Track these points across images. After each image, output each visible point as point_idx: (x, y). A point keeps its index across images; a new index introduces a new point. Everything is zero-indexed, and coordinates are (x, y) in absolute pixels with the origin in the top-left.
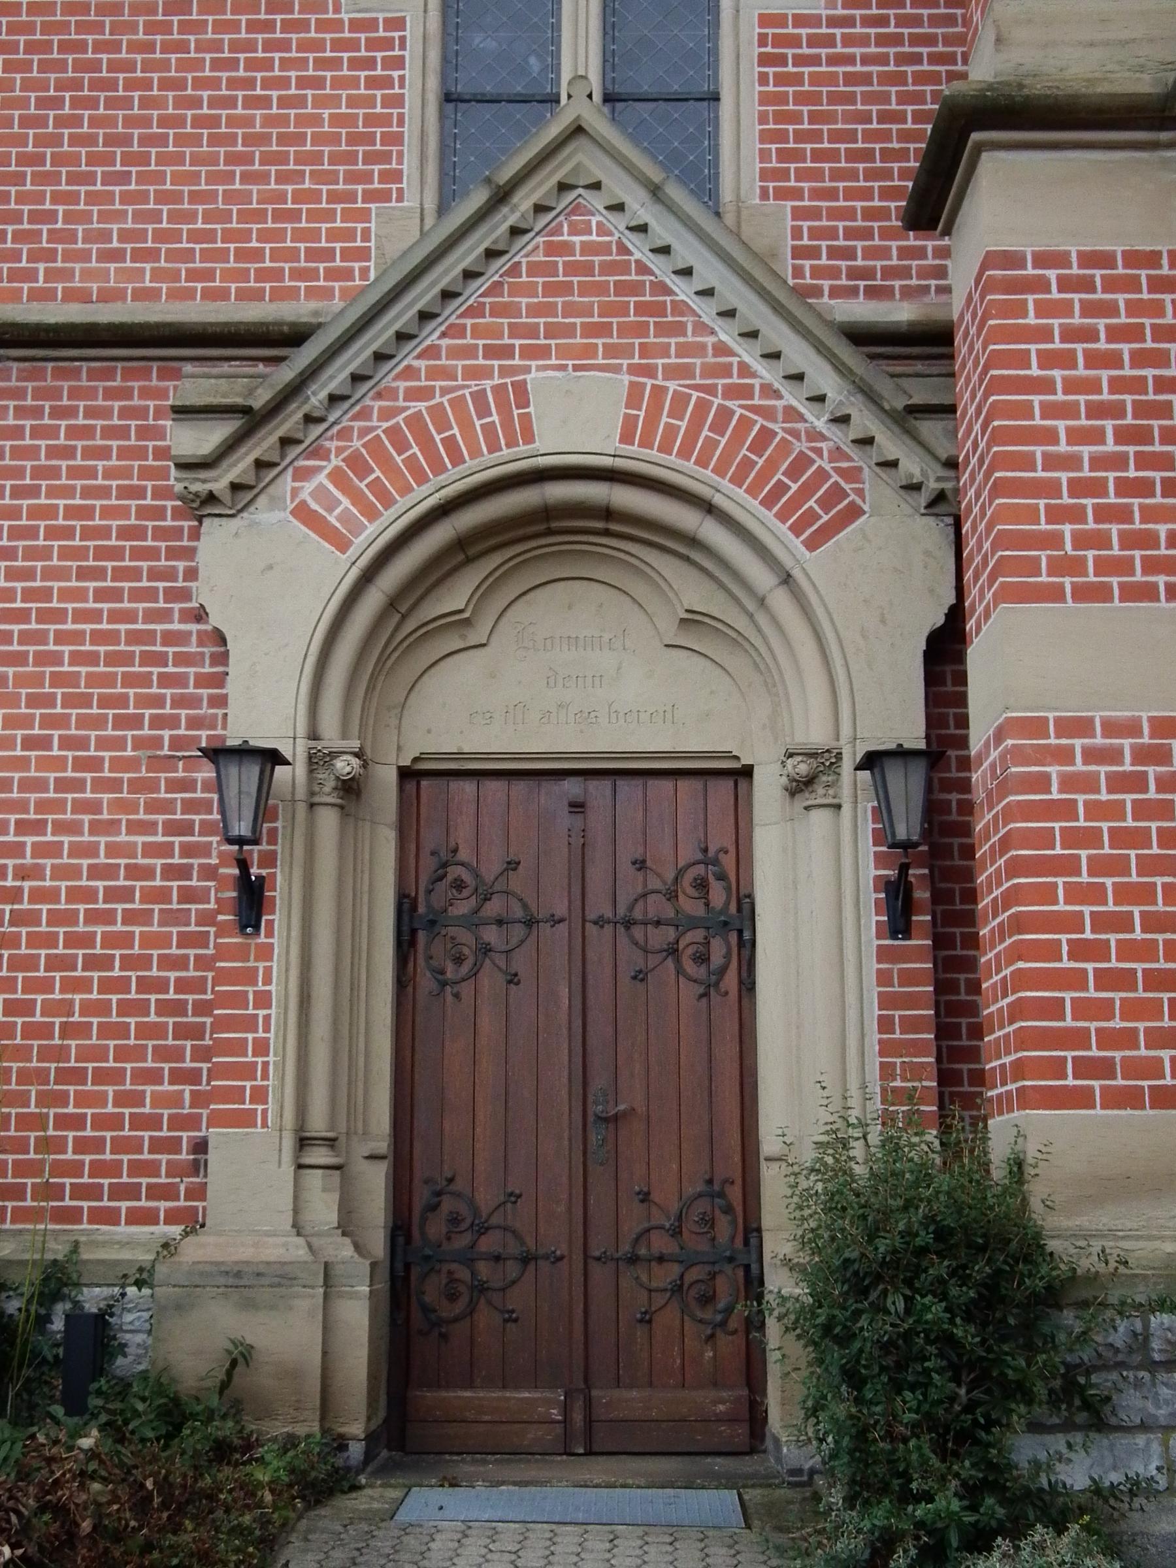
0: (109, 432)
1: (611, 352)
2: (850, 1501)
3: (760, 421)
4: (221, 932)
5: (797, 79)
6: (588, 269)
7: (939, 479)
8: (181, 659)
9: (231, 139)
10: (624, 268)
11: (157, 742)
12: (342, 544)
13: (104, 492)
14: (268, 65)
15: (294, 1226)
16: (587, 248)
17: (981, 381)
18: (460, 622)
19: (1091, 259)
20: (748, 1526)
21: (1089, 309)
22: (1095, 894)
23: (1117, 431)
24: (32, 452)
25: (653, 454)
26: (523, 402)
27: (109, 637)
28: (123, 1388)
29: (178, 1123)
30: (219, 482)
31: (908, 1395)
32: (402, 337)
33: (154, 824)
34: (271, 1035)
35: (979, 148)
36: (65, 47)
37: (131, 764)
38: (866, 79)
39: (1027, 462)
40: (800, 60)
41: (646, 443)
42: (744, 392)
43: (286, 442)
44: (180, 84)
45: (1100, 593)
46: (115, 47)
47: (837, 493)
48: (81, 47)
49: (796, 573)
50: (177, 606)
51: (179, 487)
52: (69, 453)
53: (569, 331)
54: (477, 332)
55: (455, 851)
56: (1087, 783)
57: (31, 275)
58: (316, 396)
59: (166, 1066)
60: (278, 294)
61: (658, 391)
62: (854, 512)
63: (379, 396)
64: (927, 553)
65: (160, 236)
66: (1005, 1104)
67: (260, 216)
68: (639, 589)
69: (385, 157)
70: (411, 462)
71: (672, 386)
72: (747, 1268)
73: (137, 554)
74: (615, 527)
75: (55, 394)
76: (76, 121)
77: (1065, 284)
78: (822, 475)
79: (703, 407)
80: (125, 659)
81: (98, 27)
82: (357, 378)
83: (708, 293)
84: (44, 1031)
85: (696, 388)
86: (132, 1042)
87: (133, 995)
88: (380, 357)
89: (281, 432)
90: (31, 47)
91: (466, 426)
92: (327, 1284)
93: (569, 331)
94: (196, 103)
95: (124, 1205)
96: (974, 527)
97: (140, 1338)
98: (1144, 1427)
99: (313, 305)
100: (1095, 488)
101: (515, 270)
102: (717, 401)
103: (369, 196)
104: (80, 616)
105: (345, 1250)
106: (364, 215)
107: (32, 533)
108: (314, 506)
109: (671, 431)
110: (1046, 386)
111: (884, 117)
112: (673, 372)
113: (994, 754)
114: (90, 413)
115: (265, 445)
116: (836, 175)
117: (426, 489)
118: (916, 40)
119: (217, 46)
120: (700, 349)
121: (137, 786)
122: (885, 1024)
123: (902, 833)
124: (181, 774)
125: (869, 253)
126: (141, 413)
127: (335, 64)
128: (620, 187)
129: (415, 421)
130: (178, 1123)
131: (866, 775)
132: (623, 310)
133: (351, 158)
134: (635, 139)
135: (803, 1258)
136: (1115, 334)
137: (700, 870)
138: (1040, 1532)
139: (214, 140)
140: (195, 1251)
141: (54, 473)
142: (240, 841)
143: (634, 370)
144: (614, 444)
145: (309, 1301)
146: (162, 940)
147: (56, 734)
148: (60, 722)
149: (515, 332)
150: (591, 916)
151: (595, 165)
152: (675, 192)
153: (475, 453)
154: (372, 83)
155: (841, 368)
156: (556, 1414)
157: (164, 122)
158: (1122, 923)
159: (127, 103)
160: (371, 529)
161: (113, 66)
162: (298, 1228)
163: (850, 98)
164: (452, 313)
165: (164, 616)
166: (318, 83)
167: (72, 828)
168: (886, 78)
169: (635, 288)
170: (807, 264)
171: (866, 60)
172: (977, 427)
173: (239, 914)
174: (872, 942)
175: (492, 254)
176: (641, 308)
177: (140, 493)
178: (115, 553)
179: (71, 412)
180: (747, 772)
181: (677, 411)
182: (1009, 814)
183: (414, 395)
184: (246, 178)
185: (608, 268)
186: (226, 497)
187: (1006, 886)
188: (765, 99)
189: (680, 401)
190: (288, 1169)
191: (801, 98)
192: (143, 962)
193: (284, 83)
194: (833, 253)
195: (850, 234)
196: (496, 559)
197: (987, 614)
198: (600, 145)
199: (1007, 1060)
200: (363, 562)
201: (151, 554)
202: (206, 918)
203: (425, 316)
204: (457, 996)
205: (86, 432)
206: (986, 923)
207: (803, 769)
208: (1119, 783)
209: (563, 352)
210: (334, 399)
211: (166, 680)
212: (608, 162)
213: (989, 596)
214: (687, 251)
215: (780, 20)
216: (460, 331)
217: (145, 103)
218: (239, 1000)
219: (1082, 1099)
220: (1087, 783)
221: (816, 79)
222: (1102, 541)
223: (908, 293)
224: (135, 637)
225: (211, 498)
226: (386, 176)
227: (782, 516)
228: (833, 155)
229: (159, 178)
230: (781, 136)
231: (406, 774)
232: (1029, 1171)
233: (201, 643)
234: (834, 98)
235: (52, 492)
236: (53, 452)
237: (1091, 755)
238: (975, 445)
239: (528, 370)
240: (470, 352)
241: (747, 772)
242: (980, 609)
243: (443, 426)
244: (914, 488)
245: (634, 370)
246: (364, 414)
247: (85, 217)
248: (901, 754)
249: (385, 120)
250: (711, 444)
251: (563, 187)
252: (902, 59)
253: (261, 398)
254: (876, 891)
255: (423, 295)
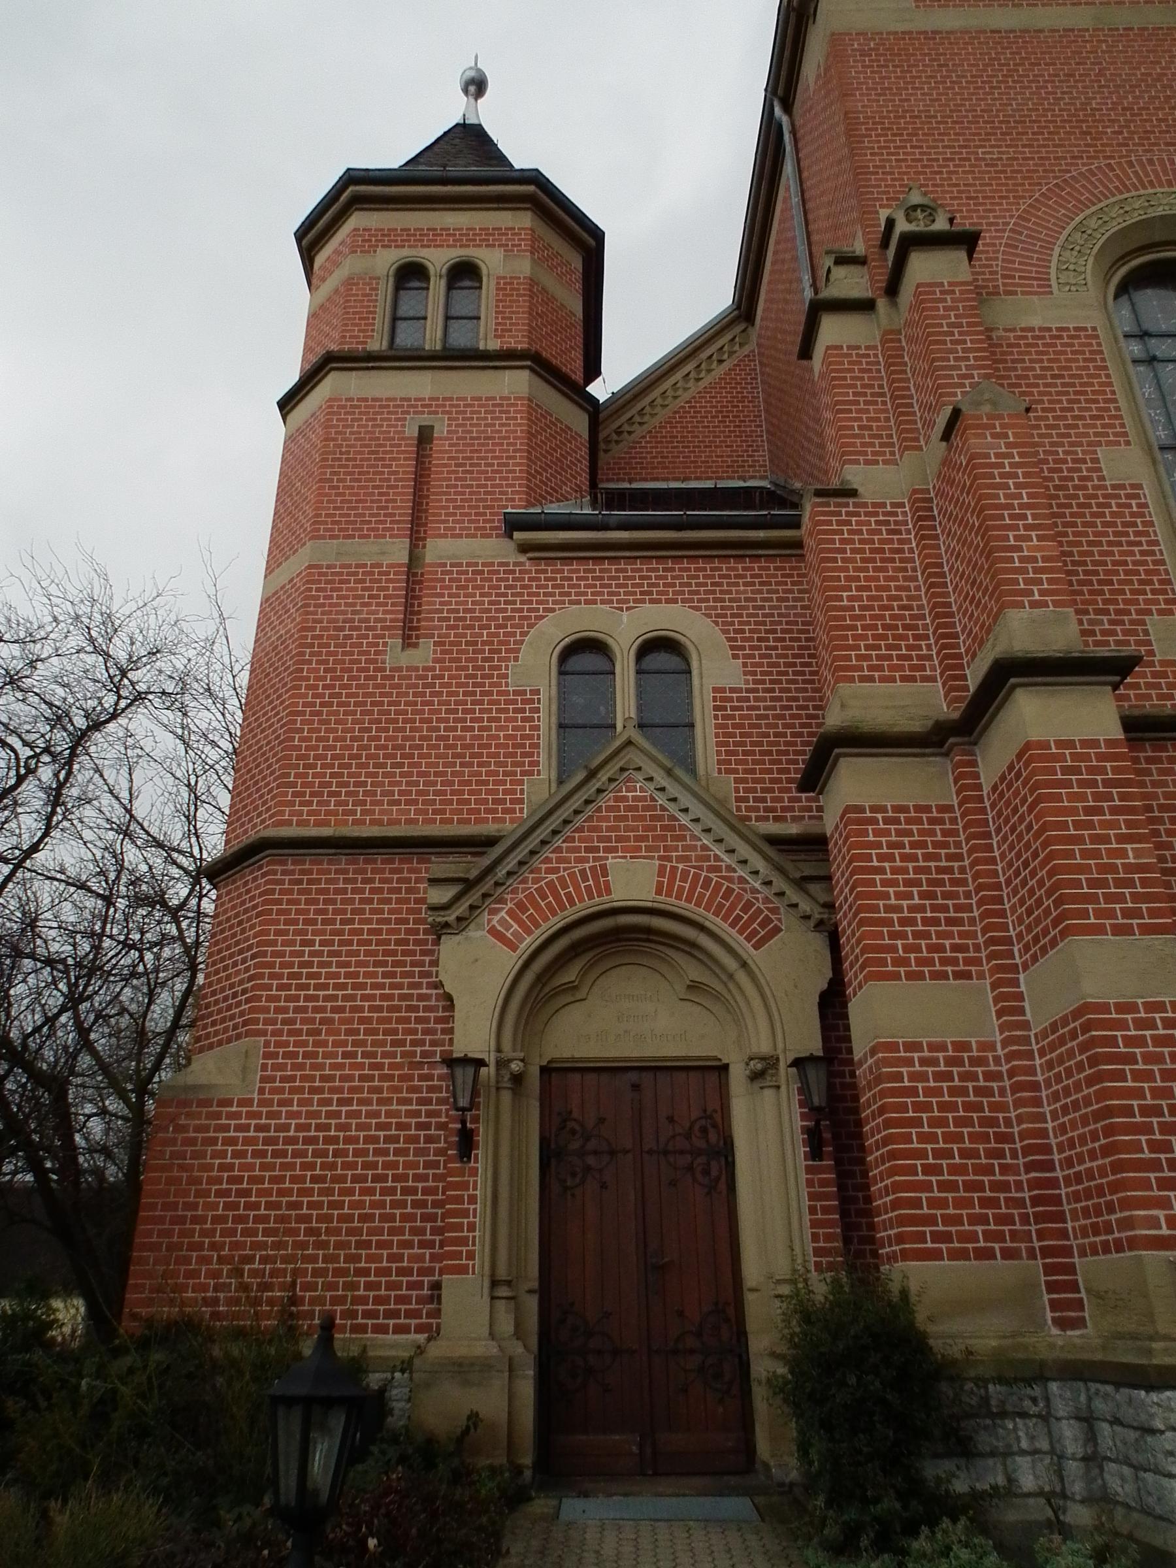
0: (391, 891)
1: (648, 849)
2: (829, 1503)
3: (726, 884)
4: (450, 1159)
5: (733, 717)
6: (636, 808)
7: (820, 913)
8: (427, 1009)
9: (454, 746)
10: (654, 808)
11: (414, 1054)
12: (514, 948)
13: (388, 921)
14: (473, 711)
15: (490, 1334)
16: (635, 798)
17: (847, 868)
18: (572, 988)
19: (898, 809)
20: (763, 1520)
21: (899, 833)
22: (932, 1138)
23: (919, 893)
24: (352, 901)
25: (673, 900)
26: (605, 874)
27: (390, 997)
28: (395, 1440)
29: (422, 1272)
30: (451, 917)
31: (861, 1436)
32: (544, 843)
33: (411, 1099)
34: (477, 1220)
35: (839, 756)
36: (373, 704)
37: (398, 1066)
38: (766, 717)
39: (875, 909)
40: (733, 708)
41: (669, 895)
42: (717, 869)
43: (485, 896)
44: (430, 721)
45: (920, 976)
46: (398, 703)
47: (766, 921)
48: (381, 703)
49: (750, 962)
50: (425, 981)
51: (430, 919)
52: (370, 901)
53: (628, 839)
54: (581, 840)
55: (571, 1112)
56: (923, 1077)
57: (354, 813)
58: (501, 872)
59: (416, 1239)
60: (477, 821)
61: (674, 869)
62: (777, 930)
63: (532, 872)
64: (816, 951)
65: (419, 793)
66: (892, 1258)
67: (469, 783)
68: (664, 968)
69: (531, 755)
70: (549, 905)
71: (681, 866)
72: (740, 1356)
73: (405, 953)
74: (696, 953)
75: (364, 871)
76: (378, 738)
77: (887, 821)
78: (759, 911)
79: (696, 877)
80: (397, 1009)
81: (390, 695)
82: (521, 863)
83: (697, 820)
84: (348, 1218)
85: (694, 867)
86: (398, 1224)
87: (399, 1197)
88: (533, 853)
89: (483, 891)
90: (356, 704)
91: (577, 888)
92: (511, 1370)
93: (628, 839)
94: (438, 729)
95: (391, 1322)
96: (848, 939)
97: (401, 1405)
98: (993, 1454)
99: (496, 826)
100: (911, 922)
101: (599, 809)
102: (704, 874)
103: (523, 773)
104: (375, 986)
105: (518, 1349)
106: (521, 782)
107: (350, 942)
108: (499, 928)
109: (681, 888)
110: (882, 871)
111: (776, 735)
112: (680, 859)
113: (870, 1061)
114: (382, 881)
115: (475, 897)
116: (754, 762)
117: (556, 919)
118: (789, 699)
119: (448, 703)
120: (694, 848)
121: (402, 1078)
122: (813, 1210)
123: (816, 1101)
124: (426, 1071)
125: (774, 800)
126: (408, 881)
127: (506, 711)
128: (651, 769)
129: (550, 884)
130: (422, 1272)
131: (794, 1070)
132: (654, 829)
133: (514, 755)
134: (654, 744)
135: (782, 1349)
136: (914, 845)
137: (703, 1122)
138: (946, 1523)
139: (446, 747)
140: (435, 1351)
141: (362, 912)
142: (463, 1110)
143: (660, 858)
144: (652, 895)
145: (499, 1382)
146: (415, 1165)
147: (360, 1050)
148: (363, 1043)
149: (600, 839)
150: (646, 1148)
151: (639, 760)
152: (679, 772)
153: (581, 900)
154: (524, 720)
155: (766, 858)
156: (635, 1449)
157: (421, 738)
158: (948, 1154)
159: (403, 729)
160: (529, 940)
161: (397, 713)
162: (492, 1336)
163: (759, 726)
164: (568, 831)
165: (418, 986)
166: (498, 720)
167: (367, 1102)
168: (775, 717)
169: (660, 818)
170: (743, 805)
171: (766, 708)
172: (847, 890)
173: (460, 1150)
174: (802, 1163)
175: (588, 802)
176: (663, 828)
177: (406, 921)
178: (393, 953)
179: (372, 881)
180: (725, 1068)
181: (684, 879)
182: (883, 1094)
183: (550, 871)
184: (462, 765)
185: (645, 808)
186: (454, 924)
187: (883, 1134)
188: (717, 726)
189: (685, 874)
190: (486, 1298)
191: (735, 726)
192: (405, 1178)
193: (481, 720)
194: (756, 800)
195: (763, 790)
196: (591, 954)
197: (860, 987)
198: (642, 751)
199: (891, 1232)
200: (525, 957)
201: (412, 953)
202: (440, 1152)
203: (555, 832)
204: (573, 1195)
205: (380, 891)
206: (872, 1153)
207: (759, 1066)
208: (939, 1076)
209: (625, 850)
210: (510, 874)
211: (419, 1020)
212: (645, 758)
213: (861, 977)
214: (686, 800)
215: (723, 690)
216: (573, 840)
217: (412, 730)
218: (459, 1200)
219: (936, 1255)
220: (923, 1077)
221: (741, 717)
222: (918, 949)
223: (794, 819)
224: (402, 997)
225: (446, 925)
226: (531, 764)
227: (741, 932)
228: (753, 753)
229: (419, 765)
230: (727, 744)
231: (543, 1070)
232: (913, 1299)
233: (437, 1000)
234: (751, 726)
235: (361, 922)
236: (362, 901)
237: (924, 1062)
238: (846, 899)
239: (607, 858)
240: (578, 850)
241: (725, 1068)
242: (855, 983)
243: (564, 887)
244: (806, 917)
245: (660, 858)
246: (525, 881)
247: (382, 784)
248: (812, 1059)
249: (531, 737)
250: (702, 896)
251: (622, 770)
252: (783, 708)
253: (474, 874)
254: (803, 1133)
255: (554, 822)
